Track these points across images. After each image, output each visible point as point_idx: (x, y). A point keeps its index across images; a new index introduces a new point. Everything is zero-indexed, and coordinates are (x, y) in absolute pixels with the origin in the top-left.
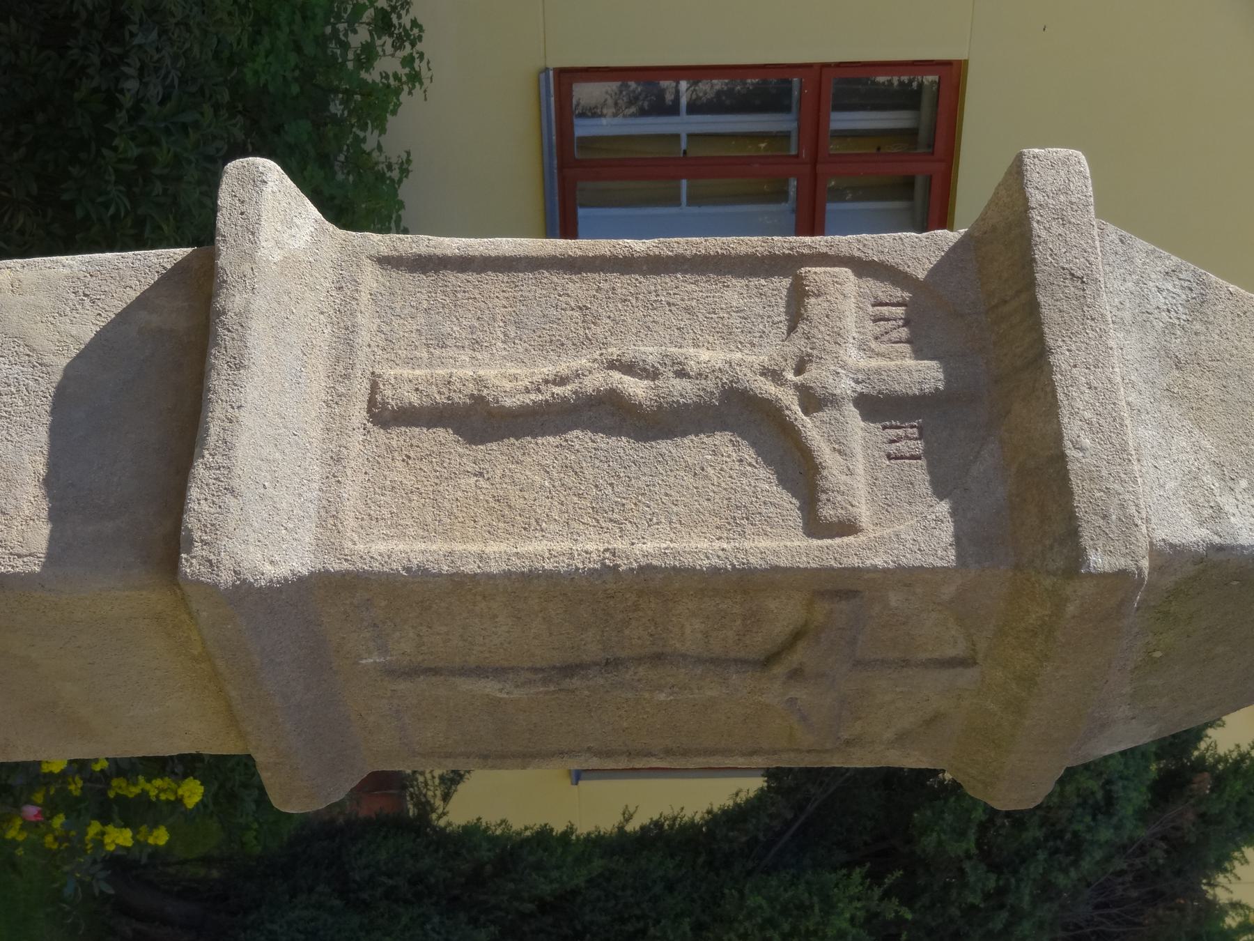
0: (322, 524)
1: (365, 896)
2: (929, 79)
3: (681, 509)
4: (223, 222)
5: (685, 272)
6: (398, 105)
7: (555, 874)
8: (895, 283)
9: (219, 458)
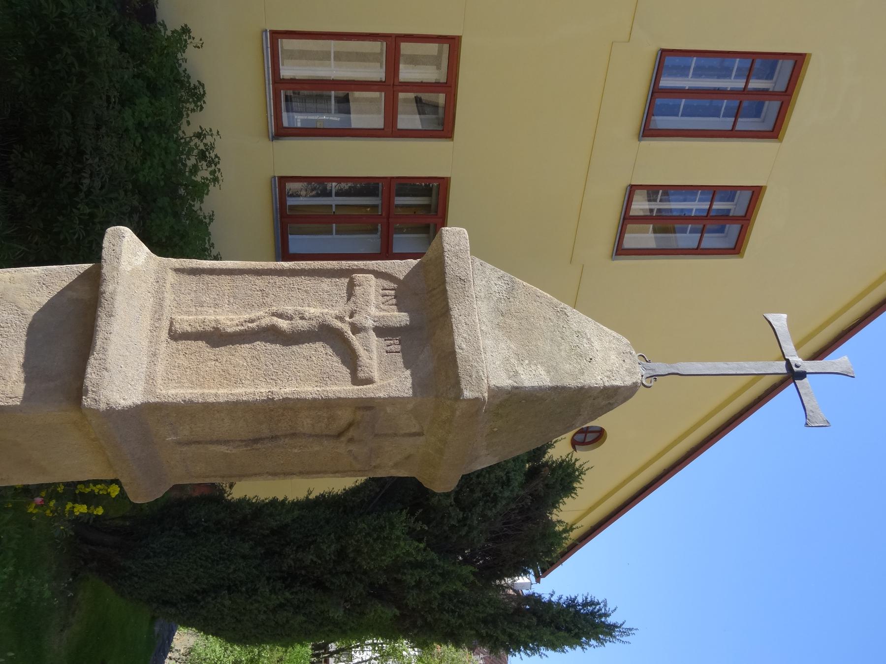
0: (147, 382)
1: (195, 531)
3: (301, 374)
4: (105, 253)
5: (305, 276)
6: (208, 191)
7: (278, 518)
8: (391, 281)
9: (101, 355)
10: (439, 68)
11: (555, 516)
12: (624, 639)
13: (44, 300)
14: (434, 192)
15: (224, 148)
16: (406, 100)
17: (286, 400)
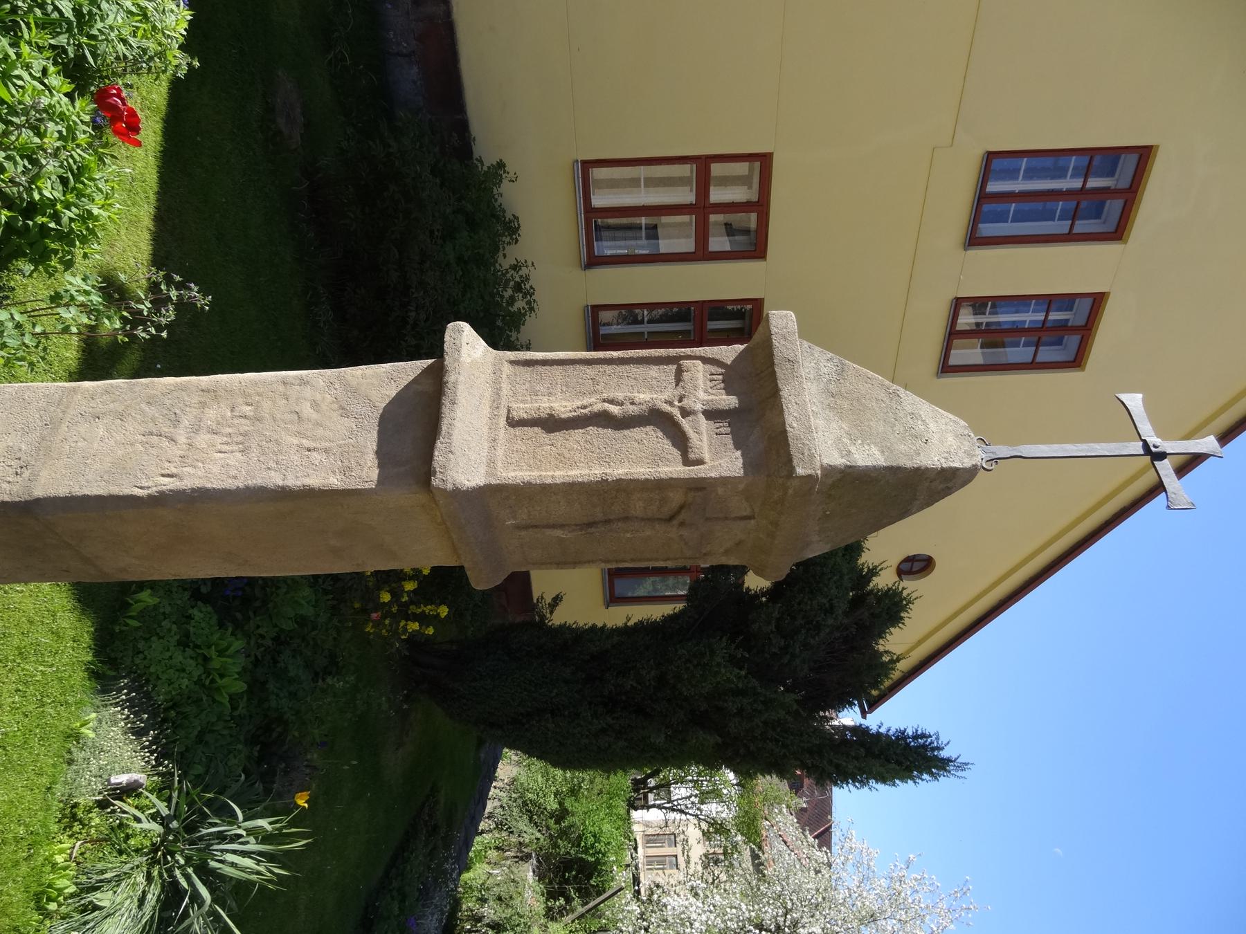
2: (749, 307)
10: (750, 187)
11: (882, 646)
12: (960, 773)
13: (393, 393)
14: (747, 318)
15: (538, 278)
16: (716, 223)
17: (619, 481)
